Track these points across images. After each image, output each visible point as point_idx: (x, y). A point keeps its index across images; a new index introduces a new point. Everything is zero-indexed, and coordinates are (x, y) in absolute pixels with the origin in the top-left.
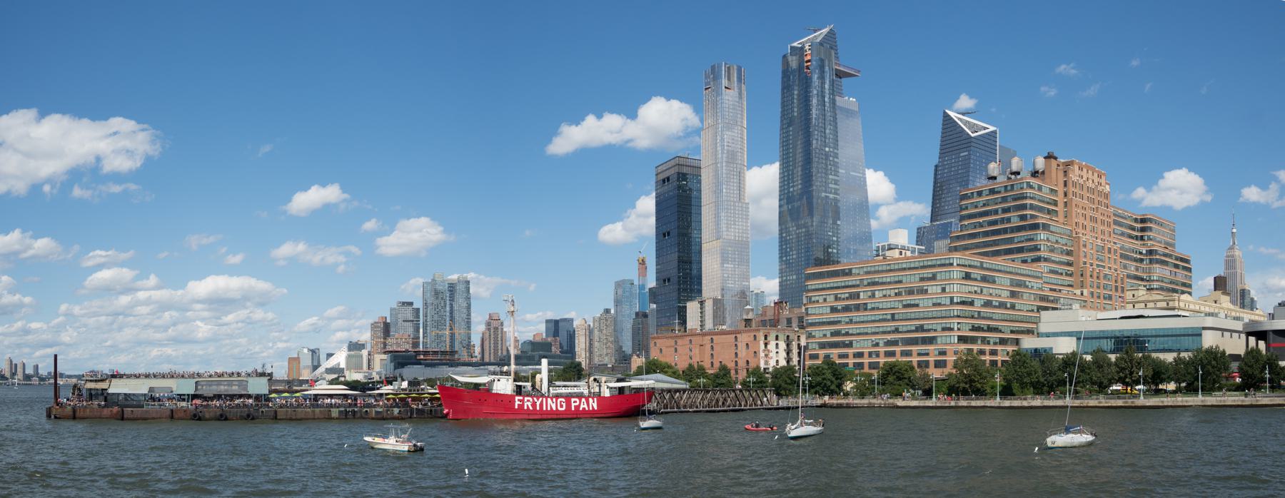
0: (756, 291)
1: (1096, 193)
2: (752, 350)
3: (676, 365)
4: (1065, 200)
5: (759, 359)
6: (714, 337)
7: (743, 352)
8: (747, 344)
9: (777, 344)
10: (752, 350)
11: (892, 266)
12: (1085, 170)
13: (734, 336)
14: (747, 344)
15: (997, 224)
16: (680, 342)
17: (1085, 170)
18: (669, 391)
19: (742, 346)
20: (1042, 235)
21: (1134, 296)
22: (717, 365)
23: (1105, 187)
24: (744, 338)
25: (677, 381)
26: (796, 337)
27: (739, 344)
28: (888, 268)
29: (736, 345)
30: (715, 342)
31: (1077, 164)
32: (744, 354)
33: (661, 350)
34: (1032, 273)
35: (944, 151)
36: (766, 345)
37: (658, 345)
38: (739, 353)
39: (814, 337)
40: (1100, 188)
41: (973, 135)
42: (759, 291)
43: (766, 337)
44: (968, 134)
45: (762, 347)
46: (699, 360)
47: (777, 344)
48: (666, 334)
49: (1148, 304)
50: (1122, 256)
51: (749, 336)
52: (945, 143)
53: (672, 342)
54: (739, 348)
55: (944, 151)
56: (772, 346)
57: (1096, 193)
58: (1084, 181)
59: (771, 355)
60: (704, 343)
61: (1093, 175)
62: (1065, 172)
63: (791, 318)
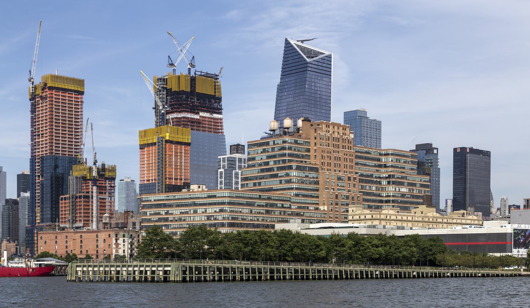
0: (126, 180)
1: (341, 141)
2: (107, 244)
3: (56, 252)
4: (315, 148)
5: (112, 249)
6: (83, 234)
7: (101, 245)
8: (104, 240)
9: (124, 240)
10: (107, 244)
11: (192, 195)
12: (331, 127)
13: (96, 234)
14: (104, 240)
15: (276, 157)
16: (59, 237)
17: (331, 127)
18: (60, 265)
19: (101, 241)
20: (294, 173)
21: (353, 210)
22: (84, 252)
23: (349, 135)
24: (103, 236)
25: (62, 261)
26: (137, 235)
27: (99, 240)
28: (190, 197)
29: (97, 240)
30: (83, 237)
31: (324, 123)
32: (102, 246)
33: (46, 242)
34: (282, 198)
35: (286, 73)
36: (116, 240)
37: (43, 238)
38: (99, 245)
39: (218, 219)
40: (345, 137)
41: (308, 60)
42: (129, 180)
43: (116, 236)
44: (305, 60)
45: (114, 241)
46: (72, 249)
47: (124, 240)
48: (52, 231)
49: (361, 216)
50: (361, 181)
51: (106, 235)
52: (286, 66)
53: (53, 236)
54: (99, 242)
55: (286, 73)
56: (120, 241)
57: (341, 141)
58: (331, 134)
59: (120, 246)
60: (76, 238)
61: (338, 128)
62: (316, 129)
63: (135, 223)
